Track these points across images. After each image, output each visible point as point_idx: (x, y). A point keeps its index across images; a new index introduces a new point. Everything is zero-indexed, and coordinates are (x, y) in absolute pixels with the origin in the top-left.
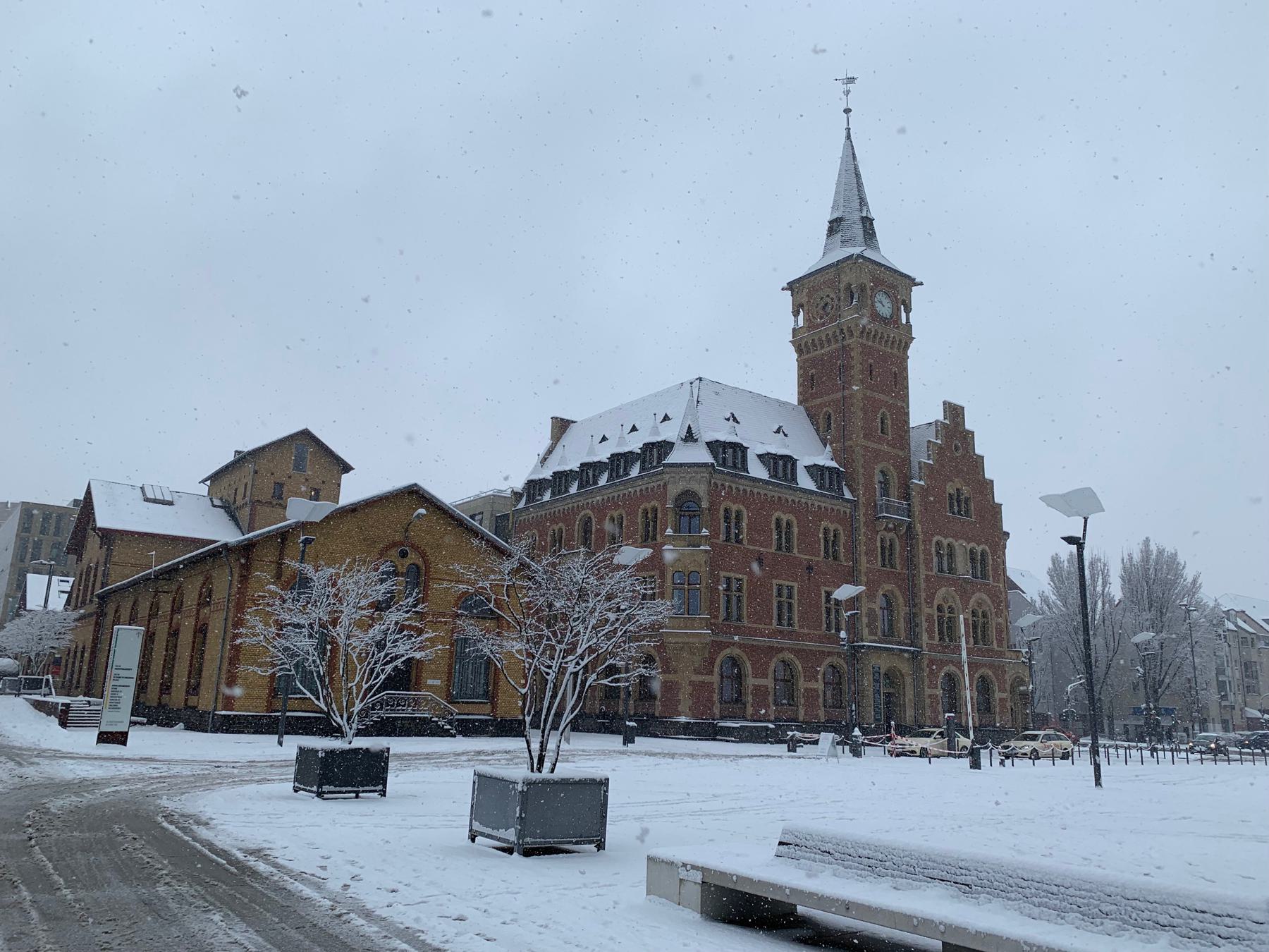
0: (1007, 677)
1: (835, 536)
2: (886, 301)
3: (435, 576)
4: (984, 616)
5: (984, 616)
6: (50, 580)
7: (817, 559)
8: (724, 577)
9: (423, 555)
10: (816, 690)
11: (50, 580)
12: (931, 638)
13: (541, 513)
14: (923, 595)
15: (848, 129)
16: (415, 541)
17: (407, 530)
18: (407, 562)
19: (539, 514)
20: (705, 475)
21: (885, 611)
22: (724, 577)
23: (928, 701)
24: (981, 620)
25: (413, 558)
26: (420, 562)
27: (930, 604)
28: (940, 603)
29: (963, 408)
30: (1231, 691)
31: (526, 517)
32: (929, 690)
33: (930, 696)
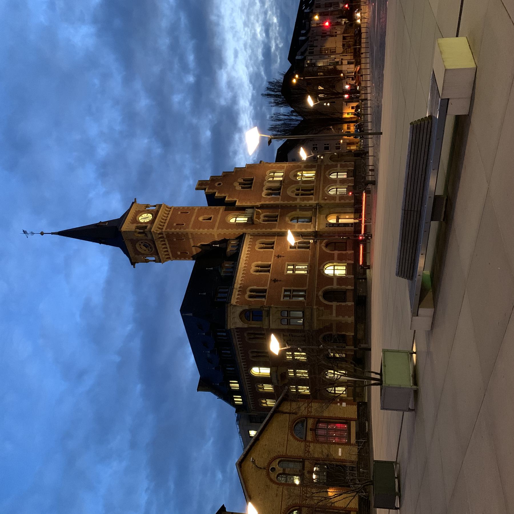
0: (330, 164)
1: (263, 244)
2: (145, 215)
3: (285, 452)
4: (298, 190)
5: (298, 190)
6: (389, 511)
7: (274, 253)
8: (284, 299)
9: (274, 459)
10: (339, 255)
11: (389, 511)
12: (311, 199)
13: (249, 397)
14: (291, 202)
15: (52, 233)
16: (266, 464)
17: (260, 468)
18: (277, 467)
19: (250, 398)
20: (232, 308)
21: (299, 220)
22: (284, 299)
23: (343, 201)
24: (300, 191)
25: (275, 465)
26: (278, 460)
27: (295, 199)
28: (294, 195)
29: (199, 181)
30: (334, 60)
31: (252, 405)
32: (337, 200)
33: (340, 200)
